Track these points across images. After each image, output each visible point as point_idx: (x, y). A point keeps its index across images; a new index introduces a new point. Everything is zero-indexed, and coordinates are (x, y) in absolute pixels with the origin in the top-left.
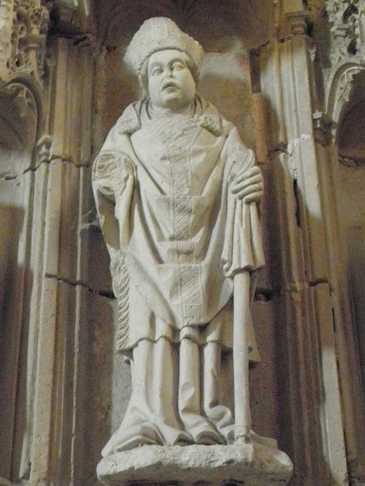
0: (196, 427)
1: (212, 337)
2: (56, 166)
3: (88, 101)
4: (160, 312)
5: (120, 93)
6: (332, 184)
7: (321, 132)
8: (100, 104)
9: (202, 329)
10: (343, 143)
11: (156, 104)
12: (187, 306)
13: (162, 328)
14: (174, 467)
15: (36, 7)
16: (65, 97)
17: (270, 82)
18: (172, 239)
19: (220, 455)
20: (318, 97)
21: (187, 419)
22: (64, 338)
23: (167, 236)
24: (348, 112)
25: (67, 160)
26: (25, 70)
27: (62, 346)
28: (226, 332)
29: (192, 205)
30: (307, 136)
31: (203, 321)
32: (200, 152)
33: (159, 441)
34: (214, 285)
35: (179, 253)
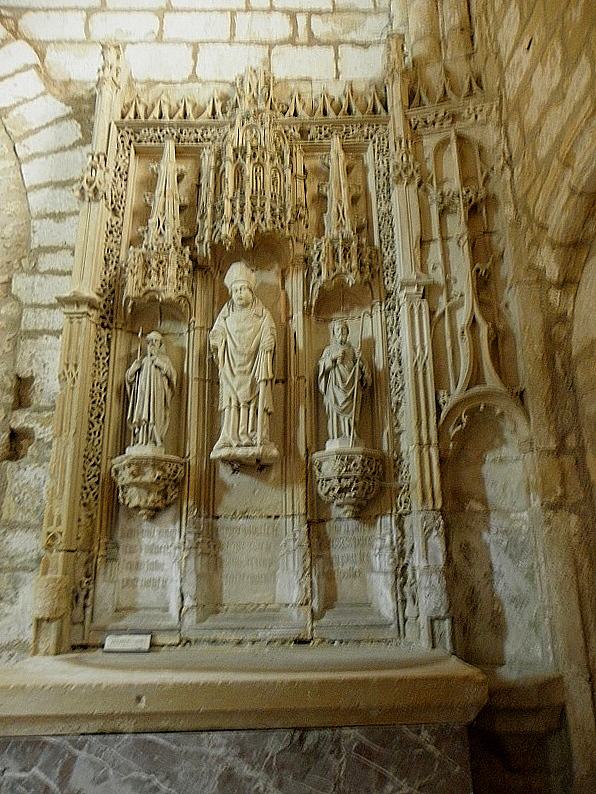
0: (245, 440)
1: (252, 405)
2: (197, 332)
3: (211, 299)
4: (233, 397)
5: (223, 297)
6: (310, 333)
7: (307, 312)
8: (216, 300)
9: (249, 403)
10: (317, 312)
11: (455, 130)
12: (243, 393)
13: (234, 403)
14: (235, 455)
15: (446, 188)
16: (200, 302)
17: (288, 285)
18: (239, 365)
19: (251, 451)
20: (307, 295)
21: (242, 438)
22: (201, 403)
23: (237, 364)
24: (318, 302)
25: (202, 328)
26: (182, 292)
27: (201, 407)
28: (257, 403)
29: (246, 352)
30: (300, 313)
31: (249, 400)
32: (251, 328)
33: (231, 446)
34: (254, 385)
35: (241, 372)
